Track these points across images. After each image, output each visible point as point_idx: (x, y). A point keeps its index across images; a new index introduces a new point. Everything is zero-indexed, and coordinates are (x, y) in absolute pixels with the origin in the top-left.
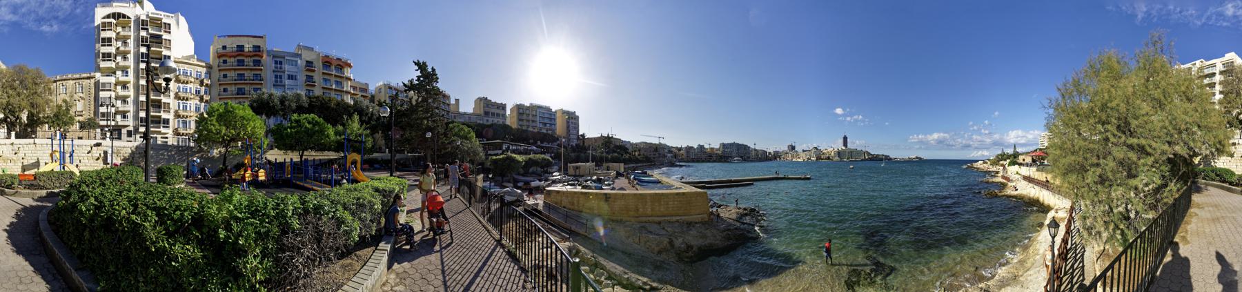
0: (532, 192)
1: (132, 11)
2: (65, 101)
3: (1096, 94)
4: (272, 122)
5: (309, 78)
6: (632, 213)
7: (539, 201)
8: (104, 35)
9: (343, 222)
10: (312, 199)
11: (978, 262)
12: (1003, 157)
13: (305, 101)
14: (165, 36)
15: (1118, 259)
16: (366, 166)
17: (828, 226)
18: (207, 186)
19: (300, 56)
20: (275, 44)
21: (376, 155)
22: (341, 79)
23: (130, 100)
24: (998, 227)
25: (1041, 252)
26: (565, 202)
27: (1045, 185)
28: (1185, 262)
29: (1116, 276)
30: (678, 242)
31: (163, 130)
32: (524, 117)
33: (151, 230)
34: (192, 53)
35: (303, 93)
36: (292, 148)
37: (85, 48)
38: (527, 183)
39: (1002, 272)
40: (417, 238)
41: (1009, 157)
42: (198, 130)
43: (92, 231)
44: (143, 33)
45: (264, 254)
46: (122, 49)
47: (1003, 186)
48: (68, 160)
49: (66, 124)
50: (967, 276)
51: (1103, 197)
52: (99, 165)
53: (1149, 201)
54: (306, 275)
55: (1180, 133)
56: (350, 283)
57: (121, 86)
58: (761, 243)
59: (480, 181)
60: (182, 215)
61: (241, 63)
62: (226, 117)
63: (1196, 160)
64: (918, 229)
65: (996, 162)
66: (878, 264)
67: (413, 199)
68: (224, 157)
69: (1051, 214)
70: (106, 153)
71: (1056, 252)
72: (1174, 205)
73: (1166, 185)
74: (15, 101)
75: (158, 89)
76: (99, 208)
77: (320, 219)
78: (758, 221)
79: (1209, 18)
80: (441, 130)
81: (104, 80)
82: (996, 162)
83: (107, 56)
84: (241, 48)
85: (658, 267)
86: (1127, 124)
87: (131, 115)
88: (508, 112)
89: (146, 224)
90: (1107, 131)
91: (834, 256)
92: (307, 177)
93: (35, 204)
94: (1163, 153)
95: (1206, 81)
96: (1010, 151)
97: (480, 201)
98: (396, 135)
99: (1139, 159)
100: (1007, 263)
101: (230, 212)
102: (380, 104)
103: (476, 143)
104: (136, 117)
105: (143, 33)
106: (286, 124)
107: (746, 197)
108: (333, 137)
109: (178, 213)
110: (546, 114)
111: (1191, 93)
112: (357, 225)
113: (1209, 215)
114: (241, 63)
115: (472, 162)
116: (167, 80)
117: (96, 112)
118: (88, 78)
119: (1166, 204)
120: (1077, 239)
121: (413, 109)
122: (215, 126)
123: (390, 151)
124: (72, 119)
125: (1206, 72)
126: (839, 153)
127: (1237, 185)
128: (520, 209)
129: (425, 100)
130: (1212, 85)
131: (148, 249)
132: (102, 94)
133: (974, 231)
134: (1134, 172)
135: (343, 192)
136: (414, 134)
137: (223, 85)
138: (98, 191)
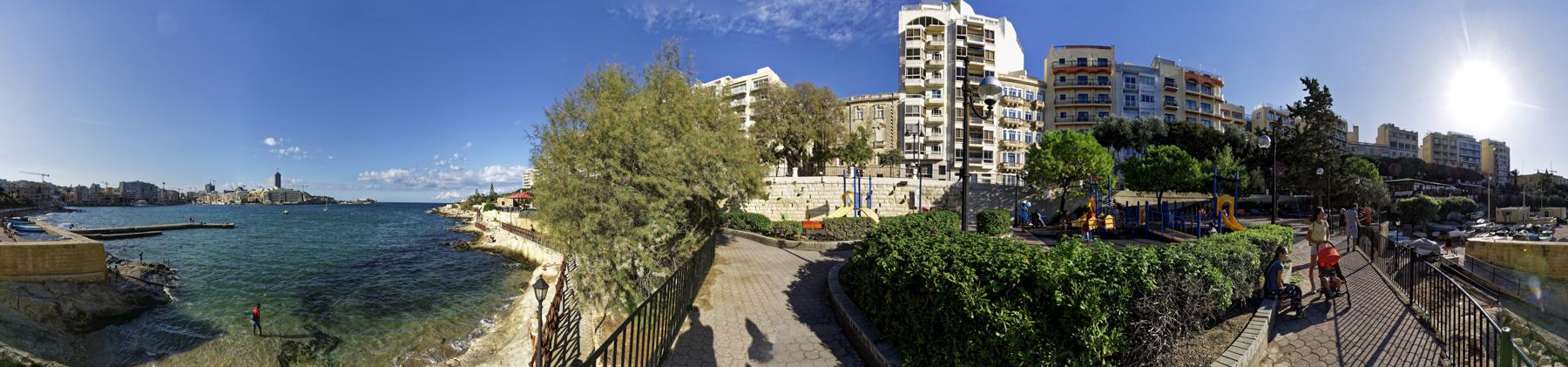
0: (1451, 243)
1: (946, 15)
2: (860, 129)
3: (594, 120)
4: (1122, 155)
5: (1169, 100)
6: (8, 271)
7: (1459, 255)
8: (910, 45)
9: (1212, 282)
10: (1173, 253)
11: (445, 333)
12: (478, 199)
13: (1164, 129)
14: (987, 47)
15: (623, 328)
16: (1241, 211)
17: (256, 286)
18: (1040, 237)
19: (1157, 71)
20: (1127, 56)
21: (1253, 197)
22: (1209, 101)
23: (944, 128)
24: (471, 289)
25: (525, 319)
26: (1492, 256)
27: (531, 235)
28: (708, 332)
29: (619, 350)
30: (67, 307)
31: (984, 165)
32: (1441, 149)
33: (970, 292)
34: (1021, 68)
35: (1161, 118)
36: (1148, 189)
37: (886, 61)
38: (1444, 232)
39: (476, 345)
40: (1305, 302)
41: (484, 199)
42: (1029, 166)
43: (895, 294)
44: (960, 43)
45: (1113, 323)
46: (933, 63)
47: (477, 236)
48: (864, 203)
49: (862, 158)
50: (432, 350)
51: (604, 250)
52: (904, 210)
53: (661, 255)
54: (1165, 350)
55: (701, 169)
56: (1221, 359)
57: (932, 110)
58: (172, 308)
59: (1385, 230)
60: (1009, 273)
61: (1083, 80)
62: (1064, 149)
63: (721, 204)
64: (370, 290)
65: (468, 206)
66: (318, 335)
67: (1301, 253)
68: (1062, 200)
69: (537, 273)
70: (912, 194)
71: (544, 320)
72: (693, 260)
73: (683, 235)
74: (798, 129)
75: (978, 114)
76: (904, 264)
77: (1183, 278)
78: (168, 280)
79: (737, 24)
80: (1336, 166)
81: (910, 102)
82: (468, 206)
83: (914, 72)
84: (1083, 61)
85: (41, 338)
86: (634, 157)
87: (944, 147)
88: (1420, 143)
89: (964, 284)
90: (608, 166)
91: (263, 324)
92: (1166, 225)
93: (823, 258)
94: (680, 194)
95: (734, 104)
96: (486, 192)
97: (1385, 255)
98: (1279, 171)
99: (649, 202)
100: (483, 333)
101: (1070, 269)
102: (1259, 133)
103: (1379, 182)
104: (951, 149)
105: (960, 43)
106: (1140, 157)
107: (154, 251)
108: (1199, 175)
109: (1004, 270)
110: (1469, 146)
111: (715, 119)
112: (1229, 285)
113: (737, 274)
114: (1083, 80)
115: (1374, 206)
116: (990, 103)
117: (900, 143)
118: (890, 100)
119: (682, 259)
120: (570, 304)
121: (1300, 139)
122: (1050, 160)
123: (1271, 193)
124: (869, 151)
125: (734, 92)
126: (270, 195)
127: (773, 235)
128: (1435, 266)
129: (1315, 127)
130: (741, 109)
131: (965, 316)
132: (908, 120)
133: (440, 293)
134: (642, 219)
135: (1212, 244)
136: (1301, 170)
137: (1060, 108)
138: (902, 243)
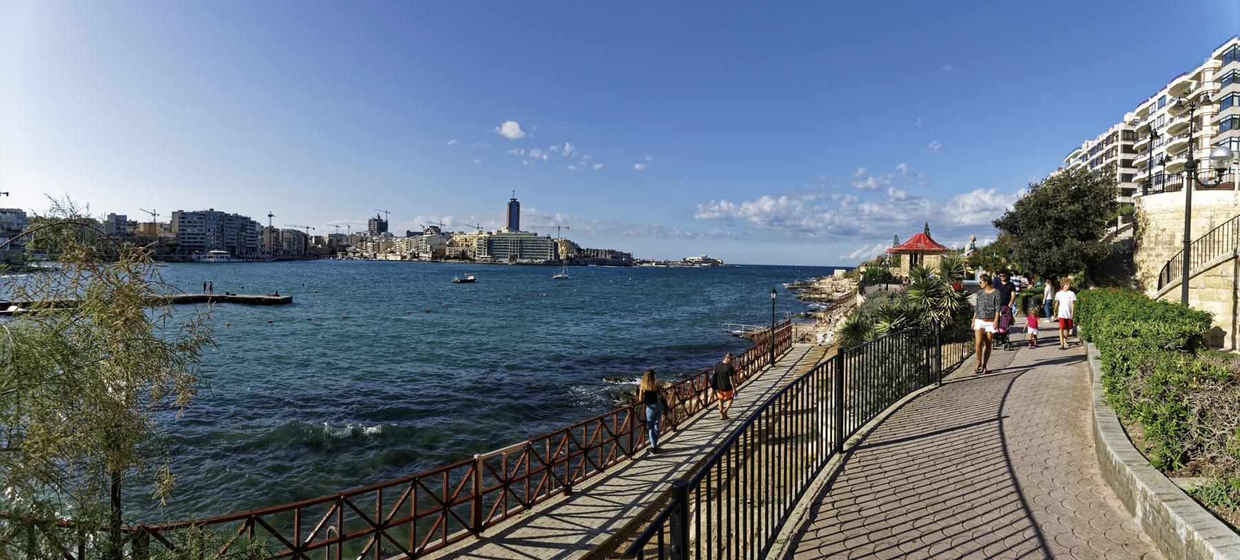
126: (491, 244)
